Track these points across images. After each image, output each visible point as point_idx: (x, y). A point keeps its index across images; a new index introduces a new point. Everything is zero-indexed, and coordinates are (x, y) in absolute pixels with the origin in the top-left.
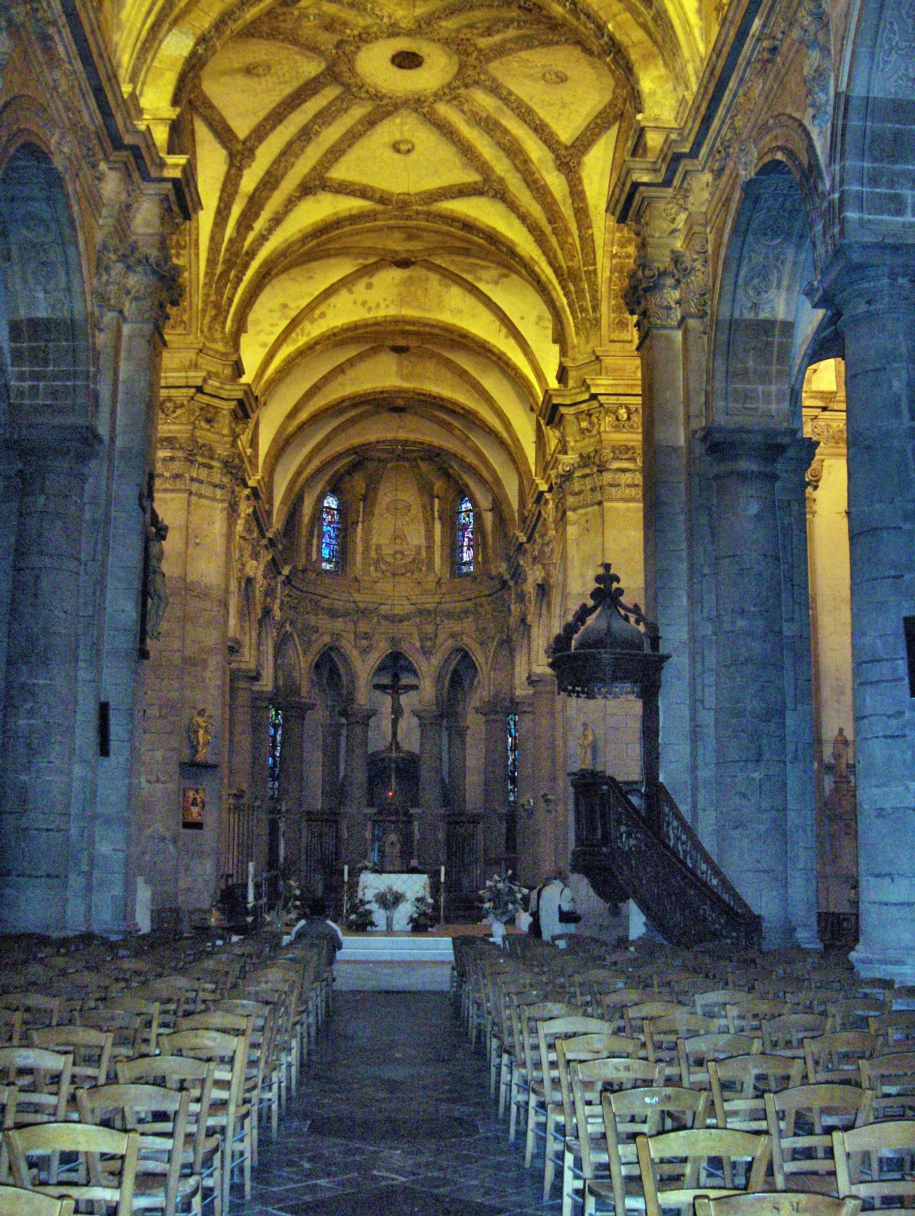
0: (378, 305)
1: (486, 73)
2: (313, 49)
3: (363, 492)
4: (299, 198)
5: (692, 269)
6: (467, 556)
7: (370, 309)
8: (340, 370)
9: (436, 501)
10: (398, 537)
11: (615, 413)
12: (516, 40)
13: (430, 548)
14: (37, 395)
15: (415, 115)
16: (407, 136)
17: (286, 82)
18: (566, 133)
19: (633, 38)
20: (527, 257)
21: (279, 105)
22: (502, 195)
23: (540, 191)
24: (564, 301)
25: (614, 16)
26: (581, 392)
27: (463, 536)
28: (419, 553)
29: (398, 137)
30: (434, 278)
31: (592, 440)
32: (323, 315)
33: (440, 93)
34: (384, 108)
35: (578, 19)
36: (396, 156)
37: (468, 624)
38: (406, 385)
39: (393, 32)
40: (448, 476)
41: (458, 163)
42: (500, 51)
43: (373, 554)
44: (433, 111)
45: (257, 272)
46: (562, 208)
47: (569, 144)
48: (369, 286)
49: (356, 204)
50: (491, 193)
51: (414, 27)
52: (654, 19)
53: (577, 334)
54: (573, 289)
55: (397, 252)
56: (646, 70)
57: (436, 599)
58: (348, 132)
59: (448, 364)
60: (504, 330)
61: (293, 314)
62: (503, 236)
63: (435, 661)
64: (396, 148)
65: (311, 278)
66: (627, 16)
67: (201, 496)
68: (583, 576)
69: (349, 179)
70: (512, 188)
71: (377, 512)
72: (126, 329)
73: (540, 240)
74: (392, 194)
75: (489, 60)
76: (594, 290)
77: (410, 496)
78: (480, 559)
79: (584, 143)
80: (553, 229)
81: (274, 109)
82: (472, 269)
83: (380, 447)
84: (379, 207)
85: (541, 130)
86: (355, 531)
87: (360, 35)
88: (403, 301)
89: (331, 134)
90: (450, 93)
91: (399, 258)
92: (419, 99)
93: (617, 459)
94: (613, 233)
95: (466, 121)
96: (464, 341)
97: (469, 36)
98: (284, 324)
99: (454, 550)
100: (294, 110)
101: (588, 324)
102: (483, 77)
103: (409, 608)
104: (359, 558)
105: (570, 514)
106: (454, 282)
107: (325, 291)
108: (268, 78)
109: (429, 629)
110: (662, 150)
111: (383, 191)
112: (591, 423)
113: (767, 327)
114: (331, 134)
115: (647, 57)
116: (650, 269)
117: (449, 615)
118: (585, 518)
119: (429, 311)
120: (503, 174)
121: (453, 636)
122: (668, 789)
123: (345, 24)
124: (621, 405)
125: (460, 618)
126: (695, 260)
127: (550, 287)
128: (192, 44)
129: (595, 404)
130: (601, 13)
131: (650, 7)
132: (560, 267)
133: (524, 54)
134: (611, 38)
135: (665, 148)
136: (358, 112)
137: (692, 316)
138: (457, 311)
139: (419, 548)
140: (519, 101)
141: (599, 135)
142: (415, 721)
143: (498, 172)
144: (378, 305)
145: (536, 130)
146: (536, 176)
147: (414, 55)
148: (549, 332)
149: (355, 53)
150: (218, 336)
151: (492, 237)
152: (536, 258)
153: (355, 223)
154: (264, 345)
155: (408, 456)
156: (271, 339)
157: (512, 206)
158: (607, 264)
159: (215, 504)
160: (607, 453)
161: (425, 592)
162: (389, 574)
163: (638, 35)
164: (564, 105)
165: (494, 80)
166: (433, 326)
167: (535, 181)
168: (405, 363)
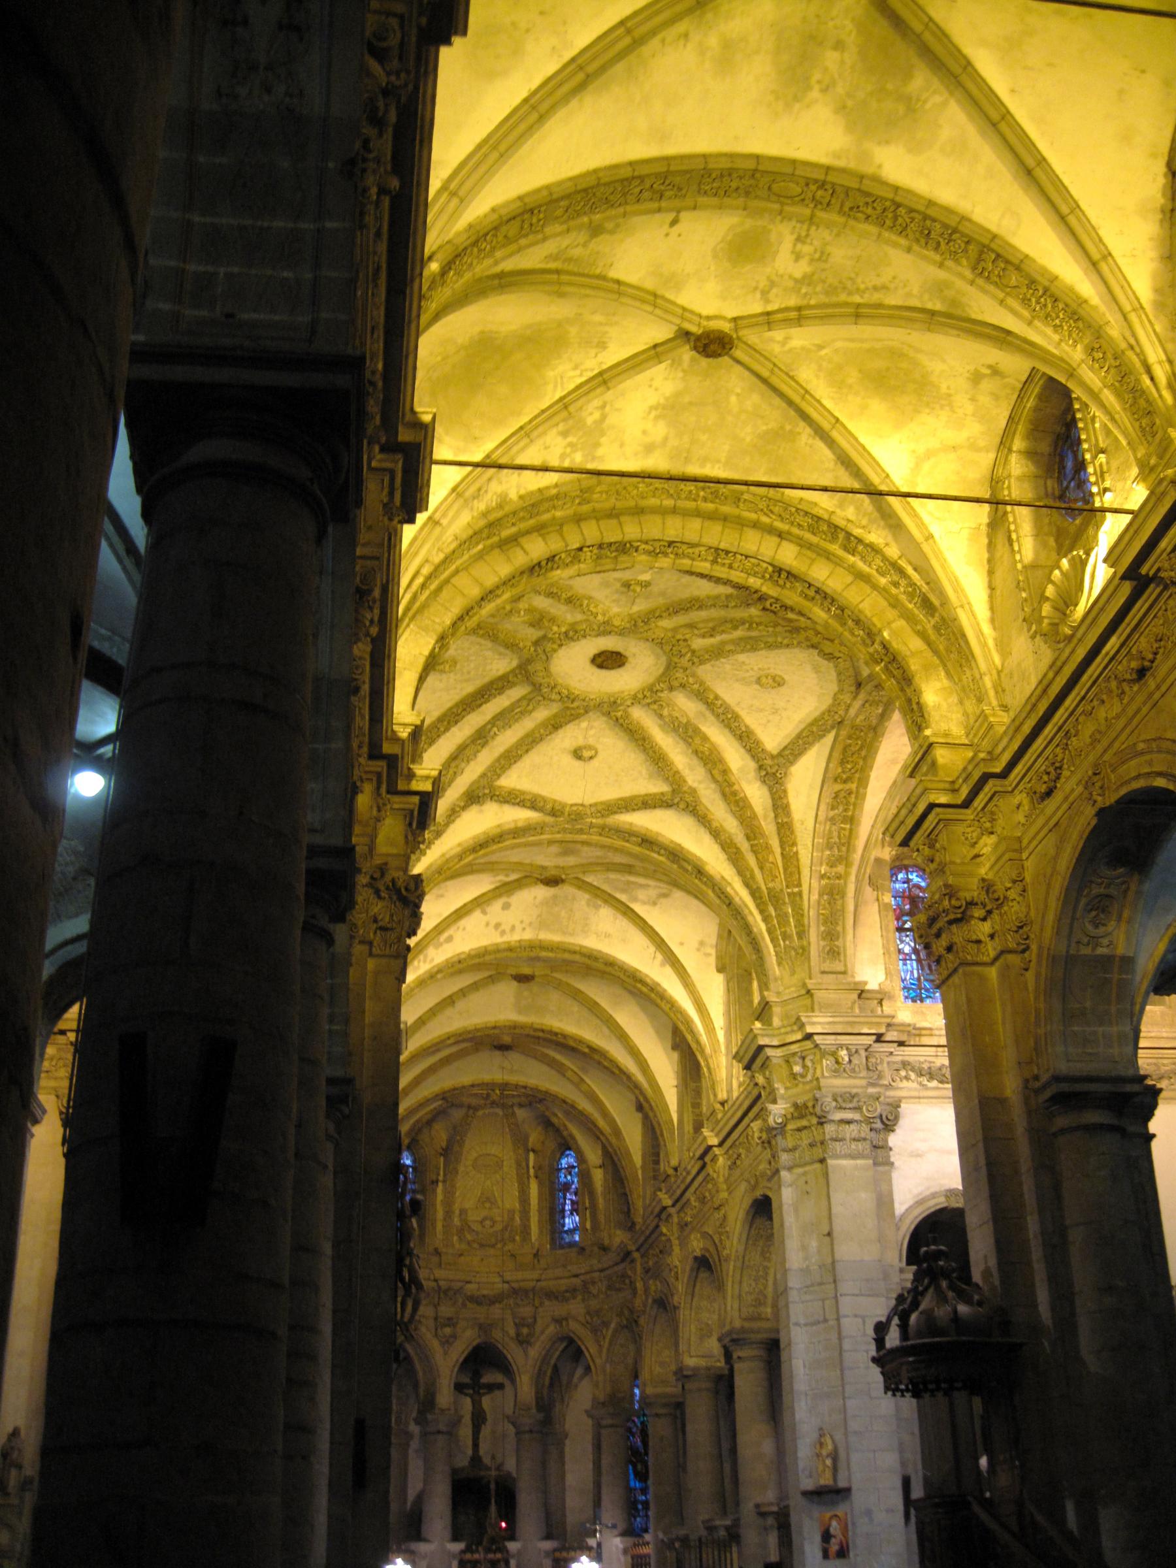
0: (513, 928)
1: (694, 675)
3: (444, 1144)
4: (464, 808)
5: (1005, 898)
6: (569, 1222)
7: (503, 933)
9: (532, 1155)
10: (487, 1199)
11: (834, 1054)
12: (737, 642)
13: (525, 1213)
15: (605, 719)
16: (591, 741)
17: (467, 680)
18: (772, 740)
19: (911, 646)
20: (717, 877)
21: (457, 705)
22: (693, 809)
24: (763, 927)
25: (889, 623)
26: (793, 1031)
27: (565, 1198)
28: (512, 1219)
29: (581, 742)
30: (583, 897)
31: (808, 1087)
33: (640, 696)
34: (573, 708)
35: (844, 624)
36: (578, 763)
37: (576, 1307)
39: (606, 629)
40: (547, 1124)
41: (644, 772)
42: (717, 653)
43: (456, 1221)
44: (627, 716)
46: (763, 823)
47: (775, 752)
48: (506, 906)
50: (682, 806)
51: (628, 625)
52: (936, 628)
53: (779, 964)
54: (773, 914)
55: (544, 868)
57: (535, 1275)
58: (527, 736)
59: (577, 996)
60: (659, 957)
62: (693, 854)
63: (534, 1352)
64: (577, 754)
65: (442, 896)
66: (902, 623)
68: (804, 1248)
69: (518, 787)
70: (704, 801)
71: (461, 1169)
73: (734, 856)
74: (564, 805)
75: (702, 663)
76: (799, 914)
77: (501, 1149)
78: (588, 1226)
80: (752, 846)
81: (451, 708)
82: (628, 888)
83: (475, 1091)
84: (549, 819)
85: (746, 739)
86: (434, 1191)
87: (566, 633)
88: (542, 925)
90: (650, 696)
91: (547, 874)
92: (615, 702)
93: (841, 1108)
94: (823, 851)
95: (660, 726)
96: (609, 969)
97: (687, 637)
99: (554, 1214)
100: (473, 710)
101: (793, 953)
102: (691, 680)
103: (500, 1287)
104: (439, 1226)
105: (784, 1174)
106: (605, 901)
107: (456, 911)
108: (452, 675)
109: (526, 1311)
110: (965, 769)
111: (555, 801)
112: (804, 1066)
113: (1106, 962)
114: (506, 739)
115: (927, 668)
116: (958, 899)
117: (551, 1295)
118: (803, 1179)
119: (572, 935)
120: (695, 785)
121: (558, 1321)
123: (553, 620)
124: (841, 1046)
126: (1007, 889)
127: (746, 912)
128: (433, 642)
129: (808, 1044)
130: (875, 620)
131: (933, 616)
132: (759, 888)
133: (742, 657)
134: (885, 646)
135: (970, 768)
136: (542, 714)
138: (608, 936)
139: (511, 1212)
140: (727, 708)
141: (811, 744)
143: (690, 782)
144: (513, 928)
145: (740, 738)
146: (736, 787)
147: (618, 654)
148: (712, 960)
149: (555, 651)
151: (676, 855)
152: (727, 877)
153: (518, 837)
155: (500, 1099)
157: (703, 819)
158: (815, 884)
160: (828, 1103)
162: (475, 1245)
163: (916, 644)
164: (775, 711)
165: (702, 683)
166: (575, 952)
167: (735, 794)
168: (526, 993)
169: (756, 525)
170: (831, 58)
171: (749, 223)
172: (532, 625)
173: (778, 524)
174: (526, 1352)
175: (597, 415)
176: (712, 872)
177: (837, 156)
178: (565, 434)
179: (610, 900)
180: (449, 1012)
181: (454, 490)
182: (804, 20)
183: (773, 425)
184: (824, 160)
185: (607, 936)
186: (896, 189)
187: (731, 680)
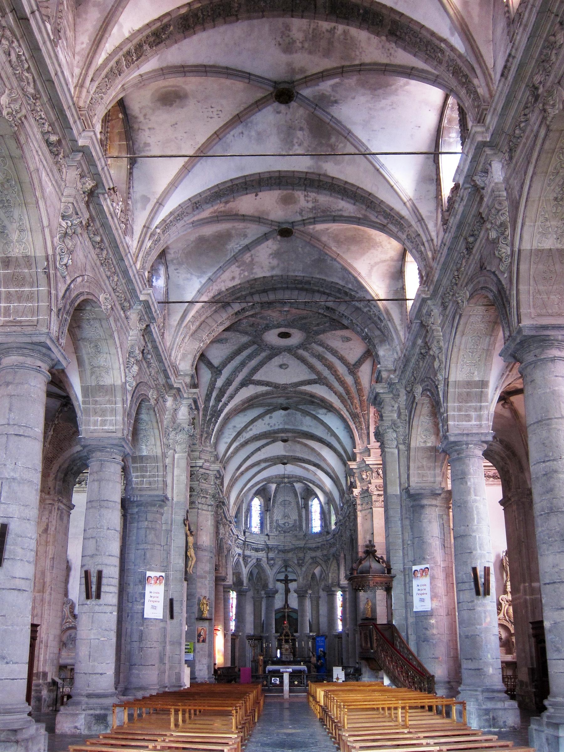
0: (275, 425)
2: (246, 333)
4: (241, 388)
8: (259, 449)
14: (143, 484)
16: (285, 362)
18: (352, 358)
20: (338, 408)
23: (342, 383)
29: (281, 363)
32: (251, 430)
34: (275, 352)
38: (287, 454)
39: (278, 326)
45: (224, 418)
48: (271, 417)
49: (264, 389)
55: (281, 404)
56: (381, 346)
61: (239, 430)
64: (281, 366)
67: (203, 510)
72: (176, 456)
73: (343, 401)
79: (360, 362)
84: (274, 390)
85: (342, 359)
88: (286, 423)
89: (253, 363)
90: (302, 346)
98: (234, 434)
104: (268, 525)
109: (301, 555)
117: (310, 549)
121: (312, 558)
122: (397, 627)
125: (315, 551)
136: (264, 354)
137: (401, 444)
139: (295, 520)
142: (296, 595)
144: (275, 425)
145: (339, 359)
147: (287, 333)
150: (208, 444)
154: (226, 443)
156: (229, 440)
157: (331, 387)
159: (209, 513)
161: (299, 539)
169: (318, 291)
170: (299, 134)
171: (285, 192)
172: (250, 326)
173: (327, 291)
174: (301, 569)
175: (250, 259)
176: (335, 406)
177: (309, 168)
178: (239, 267)
179: (308, 414)
180: (259, 453)
181: (198, 291)
182: (286, 121)
183: (316, 257)
184: (305, 170)
185: (310, 426)
186: (333, 178)
187: (334, 339)
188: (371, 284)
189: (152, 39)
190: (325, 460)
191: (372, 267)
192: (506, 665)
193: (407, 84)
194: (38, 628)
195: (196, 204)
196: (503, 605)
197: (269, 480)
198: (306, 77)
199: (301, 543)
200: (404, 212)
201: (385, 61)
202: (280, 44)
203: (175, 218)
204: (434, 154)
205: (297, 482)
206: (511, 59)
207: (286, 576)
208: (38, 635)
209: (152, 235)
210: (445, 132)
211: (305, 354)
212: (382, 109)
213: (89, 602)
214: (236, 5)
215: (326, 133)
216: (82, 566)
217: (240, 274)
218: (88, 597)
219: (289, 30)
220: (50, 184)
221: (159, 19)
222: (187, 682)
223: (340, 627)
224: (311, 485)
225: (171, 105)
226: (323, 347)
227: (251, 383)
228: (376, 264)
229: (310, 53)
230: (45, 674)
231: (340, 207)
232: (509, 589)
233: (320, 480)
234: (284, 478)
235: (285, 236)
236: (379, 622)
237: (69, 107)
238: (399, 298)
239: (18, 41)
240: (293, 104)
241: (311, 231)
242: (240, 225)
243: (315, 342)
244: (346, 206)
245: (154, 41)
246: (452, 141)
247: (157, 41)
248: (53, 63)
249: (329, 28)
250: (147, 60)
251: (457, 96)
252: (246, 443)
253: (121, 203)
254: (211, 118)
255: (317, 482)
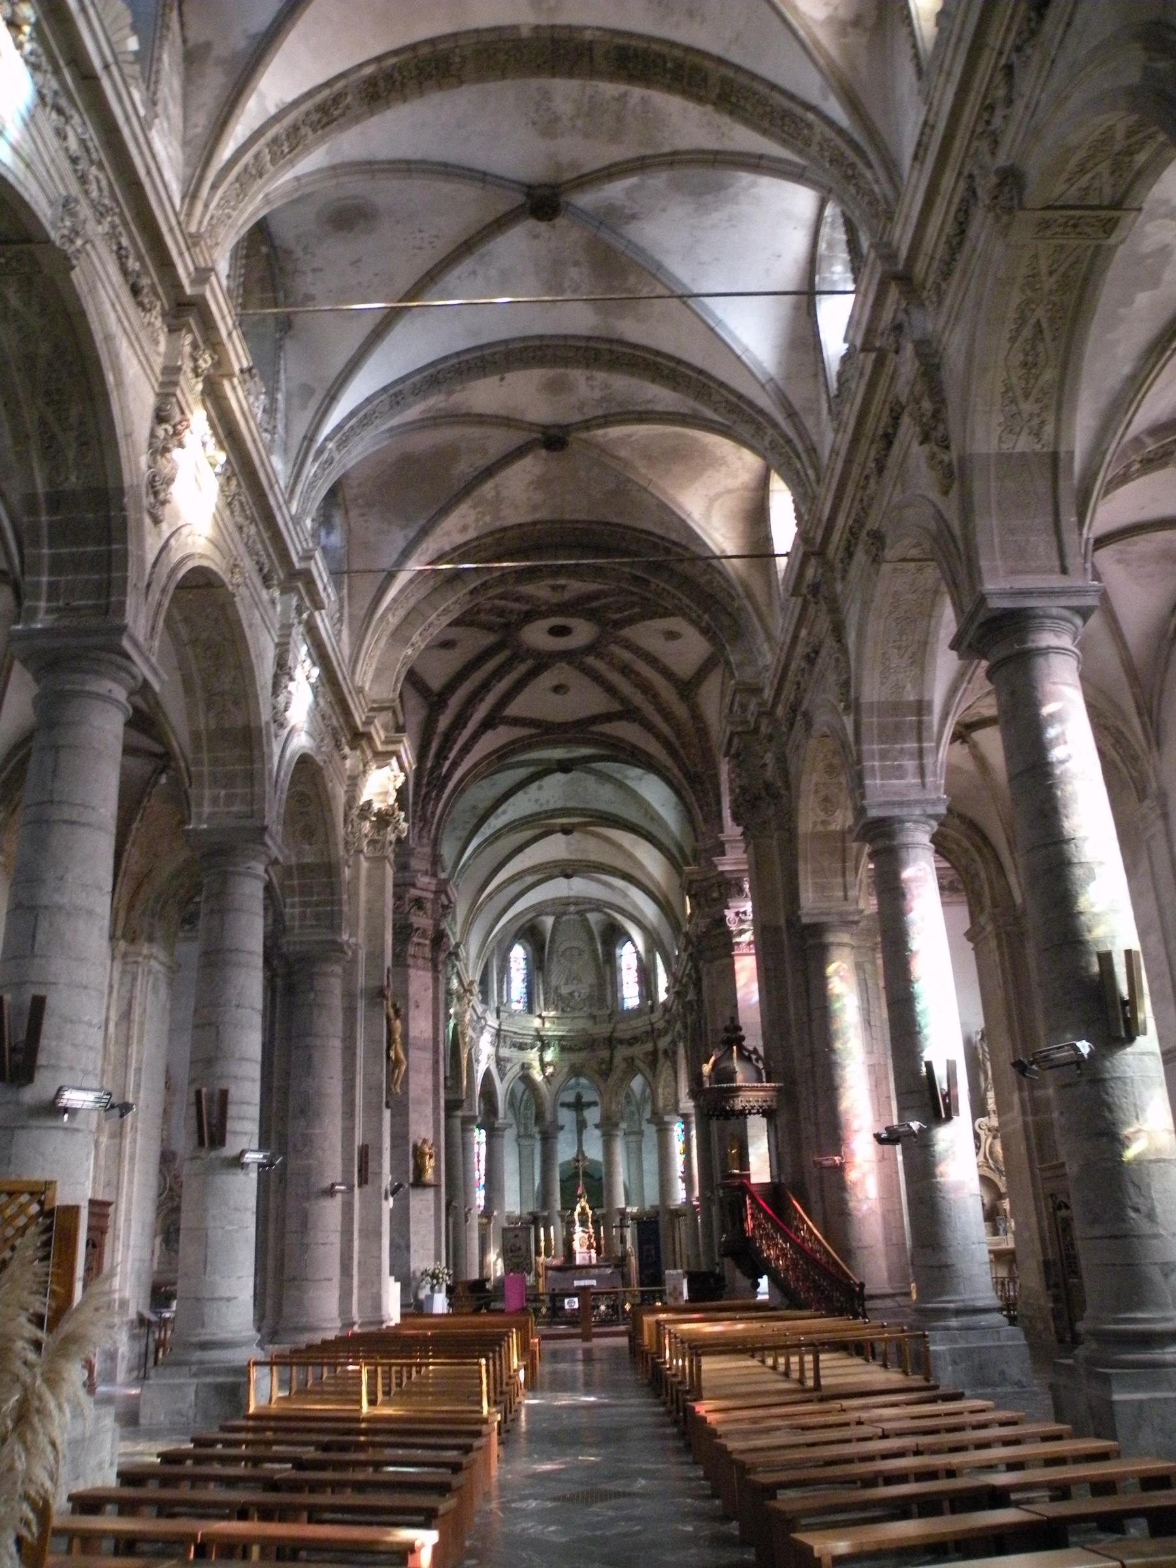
16: (563, 682)
23: (667, 715)
29: (555, 683)
32: (504, 812)
34: (543, 662)
44: (582, 663)
48: (540, 788)
90: (591, 649)
117: (621, 1042)
125: (631, 1044)
136: (522, 668)
150: (425, 841)
157: (648, 727)
170: (574, 272)
175: (493, 493)
178: (474, 507)
180: (520, 857)
187: (648, 634)
188: (711, 532)
189: (315, 117)
190: (642, 867)
191: (712, 501)
192: (999, 1257)
193: (753, 185)
194: (111, 1209)
195: (393, 395)
196: (983, 1137)
197: (540, 909)
198: (581, 177)
199: (603, 1030)
200: (764, 401)
201: (715, 145)
202: (534, 123)
203: (361, 421)
204: (806, 295)
205: (593, 910)
206: (927, 130)
207: (579, 1097)
208: (110, 1223)
209: (320, 451)
210: (824, 265)
211: (600, 666)
212: (713, 226)
213: (203, 1153)
214: (458, 60)
215: (619, 268)
216: (192, 1081)
217: (477, 520)
218: (201, 1143)
219: (550, 100)
220: (135, 362)
221: (328, 84)
222: (392, 1313)
223: (680, 1194)
224: (619, 917)
225: (351, 229)
226: (632, 651)
227: (501, 723)
228: (719, 495)
229: (586, 136)
230: (124, 1304)
231: (649, 396)
232: (991, 1105)
233: (636, 906)
234: (568, 904)
235: (555, 450)
236: (754, 1180)
237: (171, 229)
238: (759, 548)
239: (81, 115)
240: (561, 222)
241: (601, 440)
242: (474, 432)
243: (615, 643)
244: (662, 396)
245: (319, 121)
246: (838, 272)
247: (325, 120)
248: (141, 153)
249: (616, 94)
250: (308, 150)
251: (841, 201)
252: (497, 836)
253: (262, 397)
254: (420, 248)
255: (629, 908)
